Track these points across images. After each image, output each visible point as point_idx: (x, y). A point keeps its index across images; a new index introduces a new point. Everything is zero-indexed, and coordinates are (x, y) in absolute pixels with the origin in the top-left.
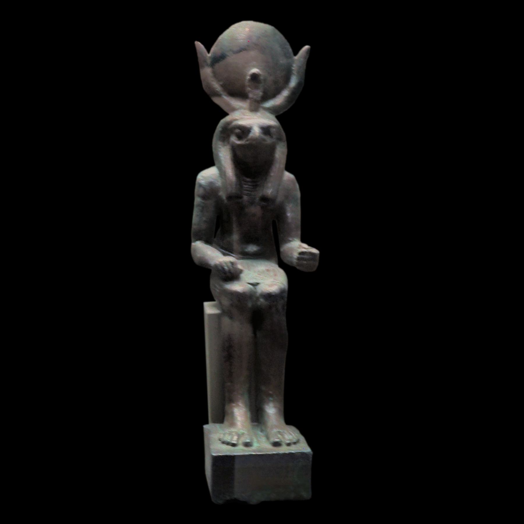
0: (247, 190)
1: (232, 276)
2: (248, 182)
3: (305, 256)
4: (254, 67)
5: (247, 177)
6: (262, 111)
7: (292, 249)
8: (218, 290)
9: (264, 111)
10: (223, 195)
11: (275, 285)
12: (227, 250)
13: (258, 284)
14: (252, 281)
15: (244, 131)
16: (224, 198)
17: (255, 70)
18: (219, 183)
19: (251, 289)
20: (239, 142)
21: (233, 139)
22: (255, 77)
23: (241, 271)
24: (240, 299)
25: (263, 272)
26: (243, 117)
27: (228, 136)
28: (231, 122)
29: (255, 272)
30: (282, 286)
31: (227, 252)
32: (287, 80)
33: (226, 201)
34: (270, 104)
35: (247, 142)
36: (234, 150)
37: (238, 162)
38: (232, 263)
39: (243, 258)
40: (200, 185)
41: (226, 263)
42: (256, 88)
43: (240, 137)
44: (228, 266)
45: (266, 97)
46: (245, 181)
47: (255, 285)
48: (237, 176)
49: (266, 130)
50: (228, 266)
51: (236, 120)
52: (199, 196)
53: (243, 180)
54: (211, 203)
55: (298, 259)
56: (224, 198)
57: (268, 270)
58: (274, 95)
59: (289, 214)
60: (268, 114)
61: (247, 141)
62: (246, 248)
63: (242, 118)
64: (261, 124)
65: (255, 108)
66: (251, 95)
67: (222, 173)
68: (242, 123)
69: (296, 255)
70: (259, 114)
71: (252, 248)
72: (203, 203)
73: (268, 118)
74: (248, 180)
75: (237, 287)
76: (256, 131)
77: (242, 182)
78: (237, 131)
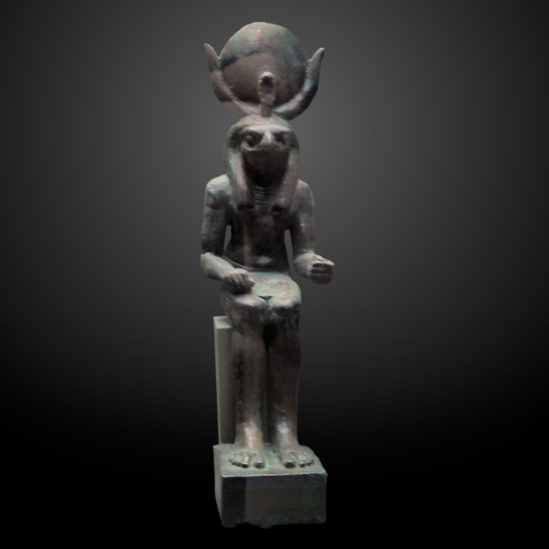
0: (259, 200)
1: (243, 289)
2: (260, 190)
3: (320, 269)
4: (266, 70)
5: (259, 185)
6: (274, 116)
7: (306, 261)
8: (228, 304)
9: (276, 117)
10: (233, 204)
11: (289, 298)
12: (238, 262)
13: (270, 297)
14: (264, 295)
15: (256, 137)
16: (235, 207)
17: (267, 74)
18: (229, 192)
19: (263, 303)
20: (250, 149)
21: (245, 146)
22: (267, 81)
23: (252, 284)
24: (252, 313)
26: (255, 122)
27: (239, 143)
28: (242, 128)
29: (267, 285)
30: (296, 300)
31: (238, 264)
32: (301, 84)
33: (236, 211)
34: (283, 109)
35: (259, 149)
36: (245, 157)
37: (250, 170)
38: (243, 276)
39: (254, 271)
40: (210, 194)
41: (237, 276)
42: (269, 92)
43: (251, 144)
44: (238, 279)
45: (278, 102)
46: (257, 190)
47: (267, 298)
48: (248, 184)
49: (279, 136)
50: (238, 279)
51: (248, 125)
52: (208, 205)
53: (255, 189)
54: (221, 212)
55: (313, 271)
56: (235, 207)
57: (281, 283)
58: (287, 100)
59: (302, 225)
60: (281, 120)
61: (259, 147)
62: (258, 260)
63: (253, 124)
64: (274, 130)
65: (267, 113)
66: (263, 100)
67: (233, 181)
68: (253, 128)
69: (310, 267)
70: (271, 119)
71: (264, 260)
72: (213, 213)
73: (280, 123)
74: (260, 188)
75: (248, 301)
76: (268, 138)
77: (254, 191)
78: (249, 137)
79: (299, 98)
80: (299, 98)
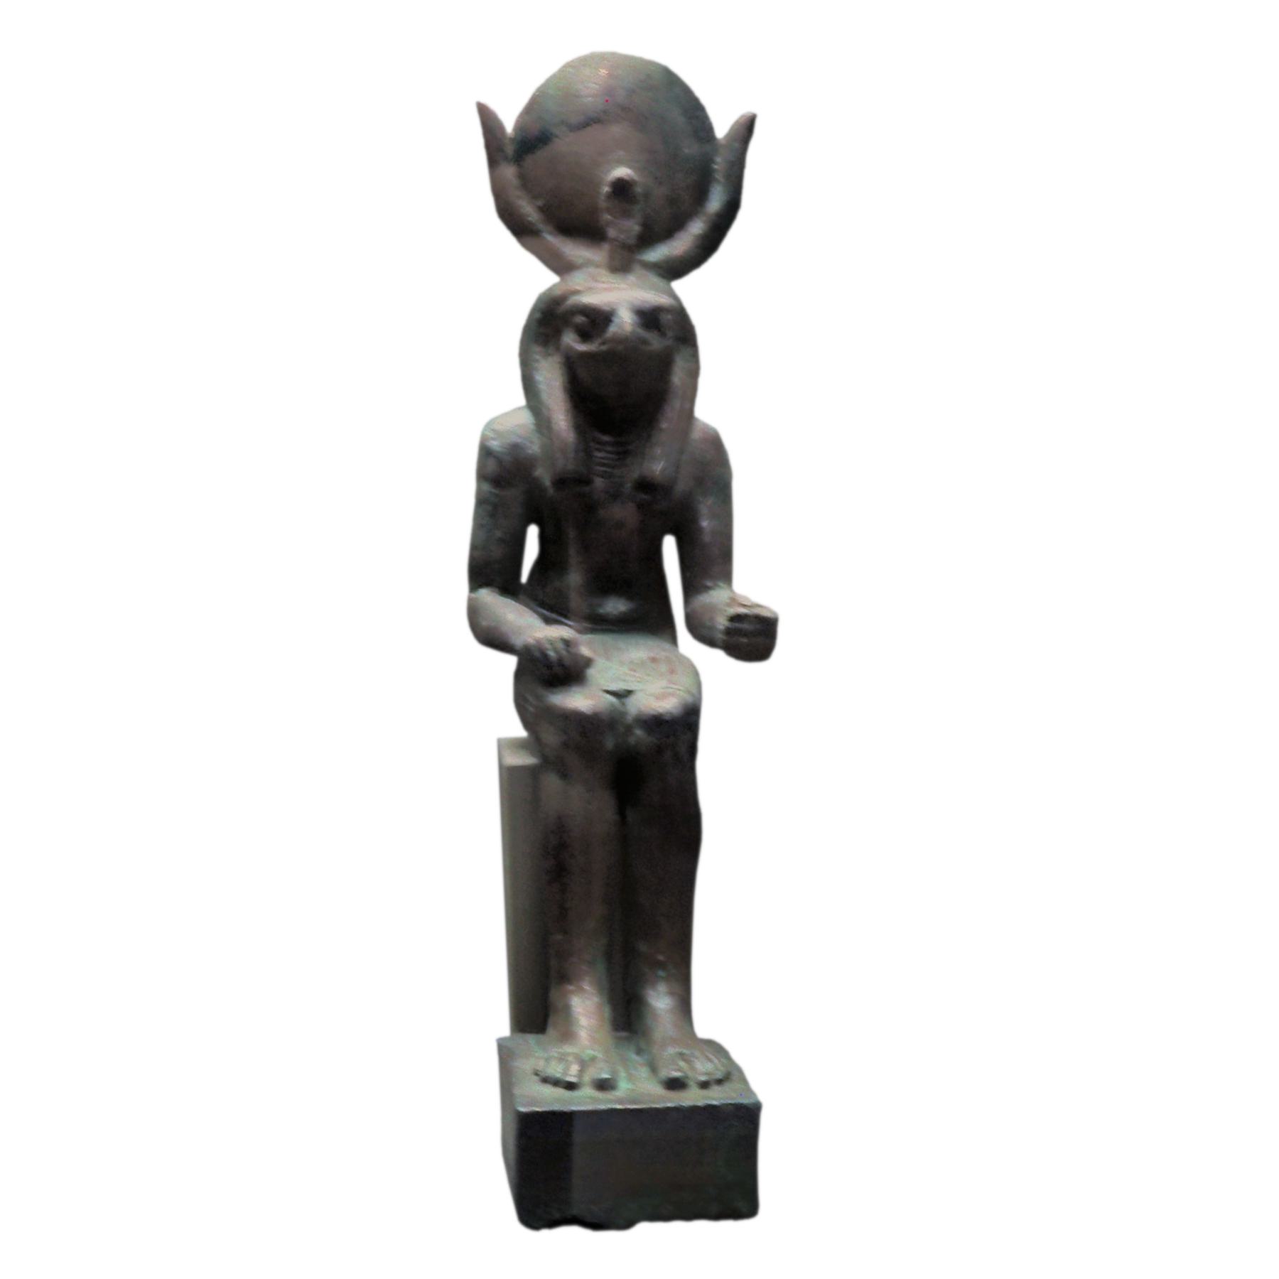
0: (604, 465)
2: (605, 443)
3: (745, 626)
4: (620, 162)
5: (604, 432)
6: (639, 271)
9: (644, 272)
10: (544, 475)
11: (672, 695)
13: (629, 693)
14: (614, 687)
15: (597, 320)
16: (547, 482)
17: (622, 172)
18: (534, 448)
19: (612, 705)
20: (582, 348)
21: (570, 339)
22: (622, 189)
23: (588, 662)
25: (642, 664)
26: (593, 284)
27: (557, 333)
29: (622, 663)
32: (701, 195)
33: (551, 491)
34: (658, 253)
35: (604, 348)
36: (572, 365)
38: (567, 643)
39: (593, 631)
41: (551, 642)
42: (626, 214)
43: (585, 335)
44: (555, 650)
45: (649, 238)
46: (599, 443)
47: (622, 695)
48: (579, 428)
50: (555, 650)
51: (577, 292)
53: (594, 440)
56: (547, 482)
57: (654, 660)
58: (668, 233)
59: (705, 524)
61: (603, 343)
62: (600, 605)
63: (590, 289)
64: (637, 303)
65: (622, 264)
66: (612, 233)
68: (590, 299)
70: (631, 278)
72: (497, 495)
74: (606, 438)
76: (625, 321)
77: (592, 444)
78: (580, 319)
79: (696, 228)
80: (696, 228)
